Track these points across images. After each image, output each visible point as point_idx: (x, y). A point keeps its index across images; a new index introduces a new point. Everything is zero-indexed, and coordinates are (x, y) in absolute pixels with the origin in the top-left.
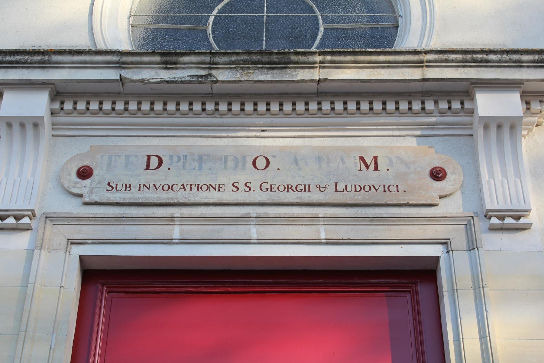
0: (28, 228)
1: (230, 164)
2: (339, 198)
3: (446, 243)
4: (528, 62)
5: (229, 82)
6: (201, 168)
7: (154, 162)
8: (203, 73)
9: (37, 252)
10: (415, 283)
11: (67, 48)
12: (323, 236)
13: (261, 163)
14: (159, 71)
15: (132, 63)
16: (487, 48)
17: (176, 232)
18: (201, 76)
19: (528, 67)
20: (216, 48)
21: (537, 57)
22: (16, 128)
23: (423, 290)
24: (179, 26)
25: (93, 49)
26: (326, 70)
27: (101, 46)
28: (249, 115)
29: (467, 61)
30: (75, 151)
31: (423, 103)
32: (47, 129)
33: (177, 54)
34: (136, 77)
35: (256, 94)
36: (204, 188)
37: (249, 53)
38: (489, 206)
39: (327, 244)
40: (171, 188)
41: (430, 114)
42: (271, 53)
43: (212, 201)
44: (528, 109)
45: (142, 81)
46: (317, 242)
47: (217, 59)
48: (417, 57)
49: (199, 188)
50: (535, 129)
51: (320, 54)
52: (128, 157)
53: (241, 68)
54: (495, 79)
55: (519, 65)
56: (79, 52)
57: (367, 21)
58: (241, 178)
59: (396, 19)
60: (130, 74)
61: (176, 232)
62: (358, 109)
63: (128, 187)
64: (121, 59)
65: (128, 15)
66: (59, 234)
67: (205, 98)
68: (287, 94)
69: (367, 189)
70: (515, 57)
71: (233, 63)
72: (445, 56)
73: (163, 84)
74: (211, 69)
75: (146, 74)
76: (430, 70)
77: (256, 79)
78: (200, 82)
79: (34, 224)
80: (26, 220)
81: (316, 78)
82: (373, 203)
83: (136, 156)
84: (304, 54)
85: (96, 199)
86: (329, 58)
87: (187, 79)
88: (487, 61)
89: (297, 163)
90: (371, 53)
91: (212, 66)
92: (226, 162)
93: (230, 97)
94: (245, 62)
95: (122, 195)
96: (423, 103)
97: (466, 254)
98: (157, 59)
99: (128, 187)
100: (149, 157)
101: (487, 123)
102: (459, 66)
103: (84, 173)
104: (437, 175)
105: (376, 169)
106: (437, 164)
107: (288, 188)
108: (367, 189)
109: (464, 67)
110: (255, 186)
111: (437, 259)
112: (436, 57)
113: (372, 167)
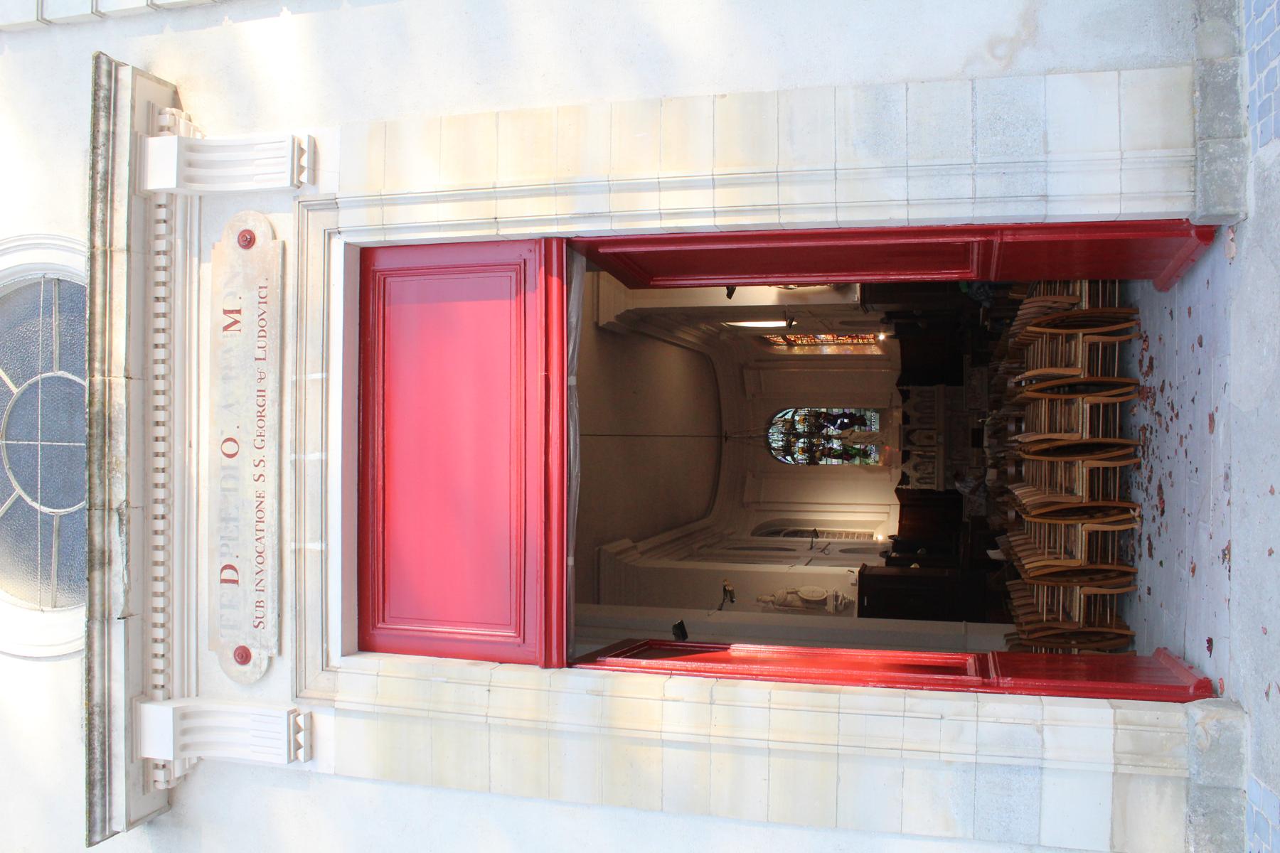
0: (310, 717)
1: (230, 484)
2: (273, 357)
3: (329, 234)
4: (109, 125)
5: (128, 486)
6: (235, 520)
7: (229, 574)
8: (115, 518)
9: (337, 705)
10: (375, 272)
11: (85, 685)
12: (318, 376)
13: (229, 447)
14: (113, 573)
15: (103, 605)
16: (88, 172)
17: (313, 546)
18: (121, 520)
19: (115, 124)
20: (83, 504)
21: (102, 114)
22: (187, 739)
23: (382, 262)
24: (54, 549)
25: (84, 654)
26: (114, 368)
27: (81, 644)
28: (170, 463)
29: (106, 197)
30: (216, 668)
31: (158, 253)
32: (190, 704)
33: (91, 551)
34: (122, 600)
35: (144, 454)
36: (260, 514)
37: (90, 462)
38: (287, 183)
39: (327, 371)
40: (260, 554)
41: (171, 245)
42: (90, 435)
43: (276, 506)
44: (169, 129)
45: (126, 592)
46: (326, 383)
47: (98, 501)
48: (98, 256)
49: (260, 520)
50: (195, 123)
51: (92, 375)
52: (223, 606)
53: (110, 472)
54: (130, 164)
55: (112, 136)
56: (89, 670)
57: (51, 316)
58: (249, 471)
59: (48, 282)
60: (118, 609)
61: (313, 546)
62: (164, 330)
63: (259, 604)
64: (98, 619)
65: (40, 613)
66: (316, 680)
67: (151, 514)
68: (144, 417)
69: (263, 323)
70: (101, 139)
71: (102, 482)
72: (97, 224)
73: (131, 568)
74: (110, 509)
75: (118, 588)
76: (115, 243)
77: (124, 454)
78: (128, 521)
79: (304, 710)
80: (301, 720)
81: (123, 380)
82: (280, 321)
83: (222, 596)
84: (91, 394)
85: (274, 640)
86: (97, 365)
87: (124, 538)
88: (106, 173)
89: (230, 406)
90: (92, 314)
91: (106, 507)
92: (229, 490)
93: (148, 486)
94: (101, 468)
95: (270, 611)
96: (158, 253)
97: (342, 213)
98: (97, 575)
99: (259, 604)
100: (223, 581)
101: (185, 178)
102: (112, 208)
103: (243, 656)
104: (247, 240)
105: (239, 312)
106: (234, 240)
107: (261, 417)
108: (263, 323)
109: (112, 201)
110: (258, 455)
111: (347, 245)
112: (98, 235)
113: (236, 316)
